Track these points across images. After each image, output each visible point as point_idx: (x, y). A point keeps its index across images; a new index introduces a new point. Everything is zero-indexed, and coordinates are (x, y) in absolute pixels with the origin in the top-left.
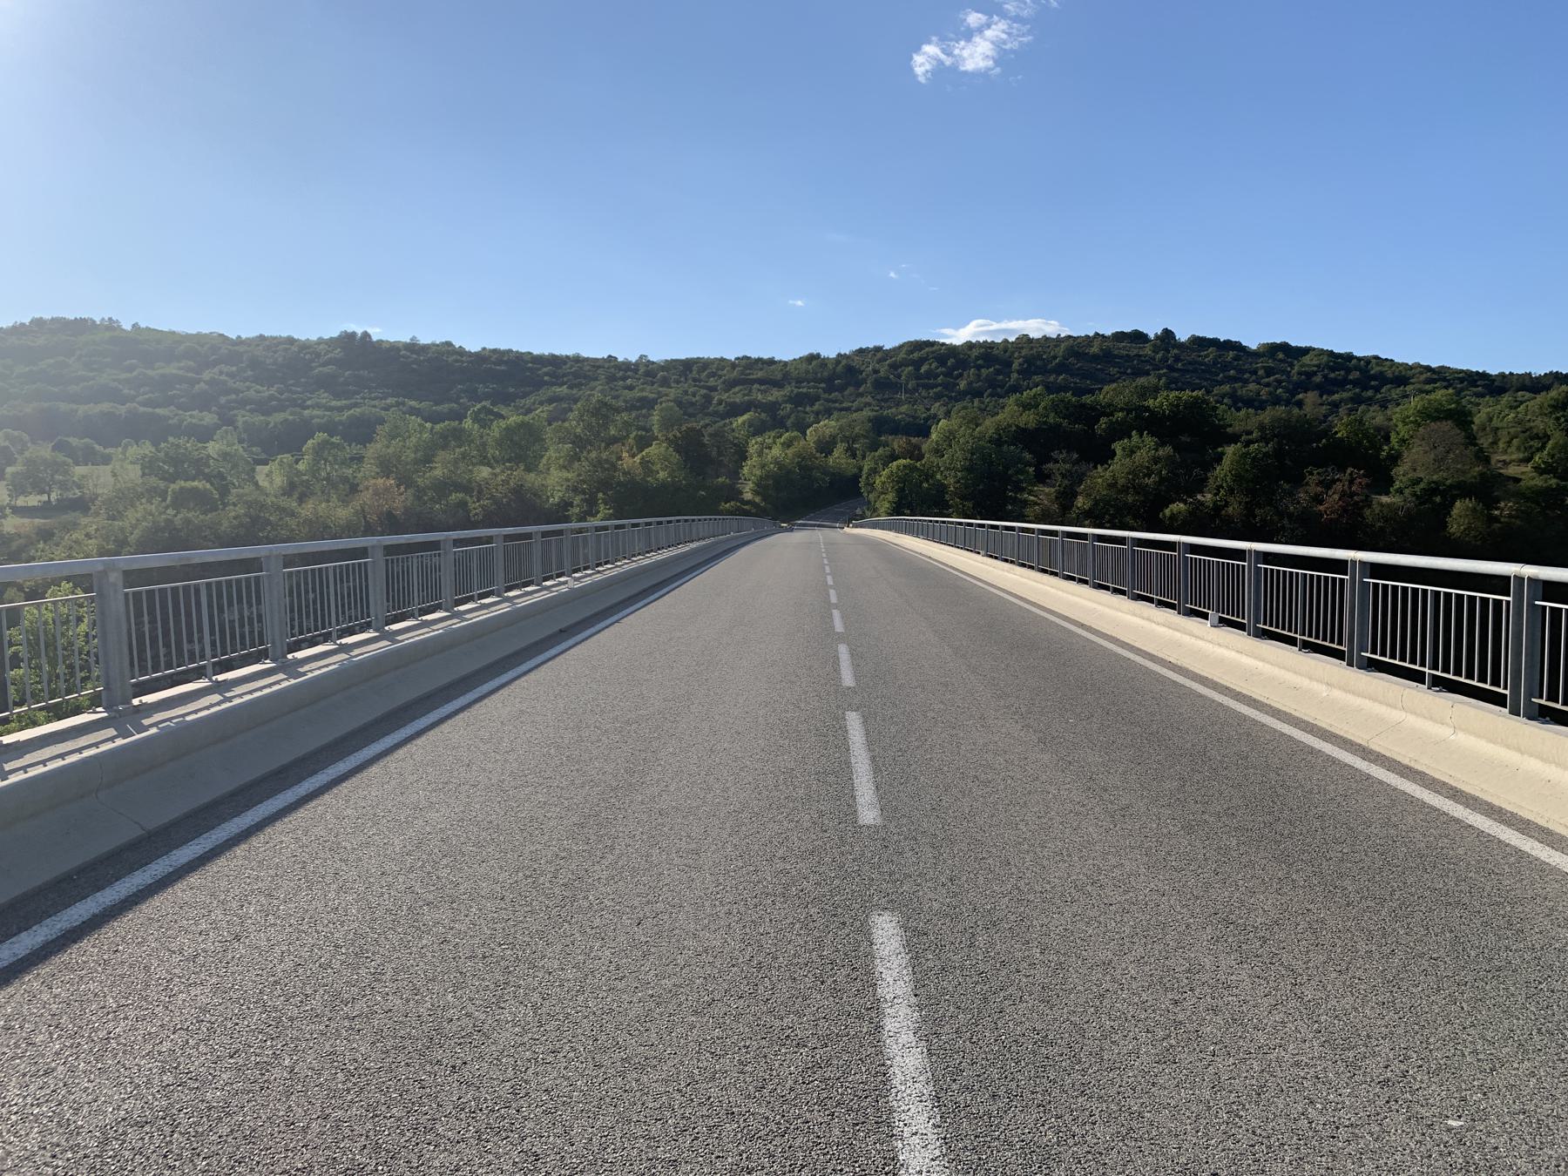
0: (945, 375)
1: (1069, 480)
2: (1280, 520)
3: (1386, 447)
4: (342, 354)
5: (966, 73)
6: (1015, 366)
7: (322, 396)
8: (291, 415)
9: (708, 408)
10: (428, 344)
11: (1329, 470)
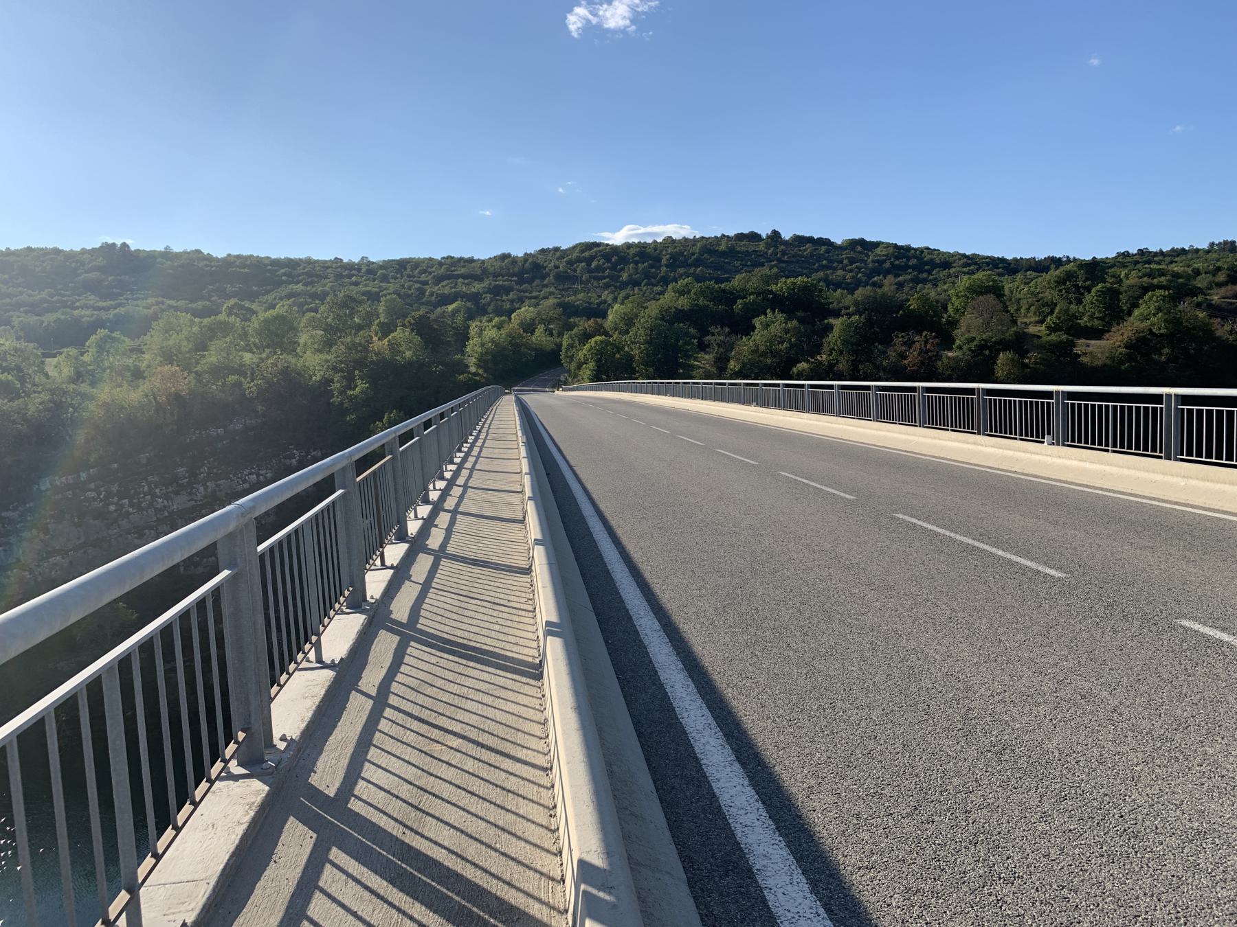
3: (945, 316)
4: (105, 262)
5: (608, 30)
6: (664, 261)
7: (90, 298)
8: (63, 315)
10: (180, 252)
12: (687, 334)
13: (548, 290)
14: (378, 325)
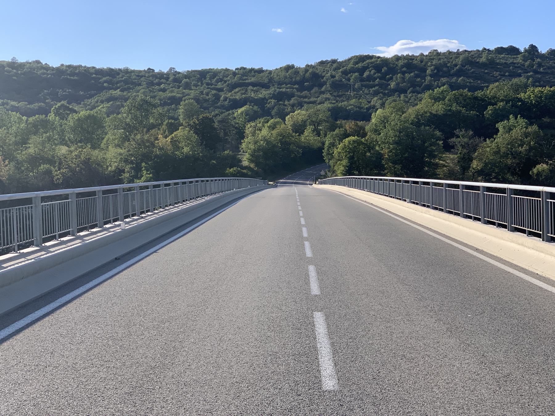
6: (429, 72)
9: (218, 103)
10: (24, 63)
12: (433, 136)
13: (324, 96)
14: (167, 125)
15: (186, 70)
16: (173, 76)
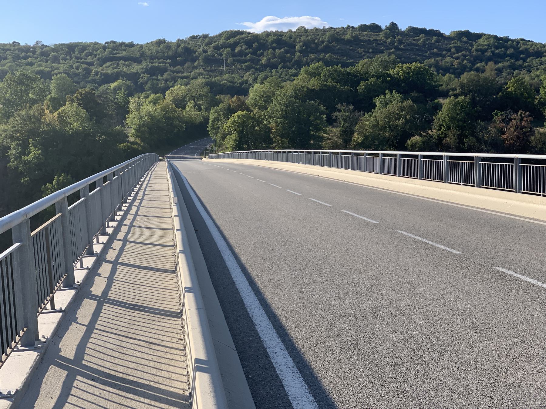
0: (252, 54)
1: (349, 123)
2: (480, 145)
3: (538, 97)
6: (297, 48)
9: (89, 77)
11: (508, 112)
12: (317, 110)
13: (198, 71)
14: (50, 100)
15: (54, 43)
16: (41, 50)
